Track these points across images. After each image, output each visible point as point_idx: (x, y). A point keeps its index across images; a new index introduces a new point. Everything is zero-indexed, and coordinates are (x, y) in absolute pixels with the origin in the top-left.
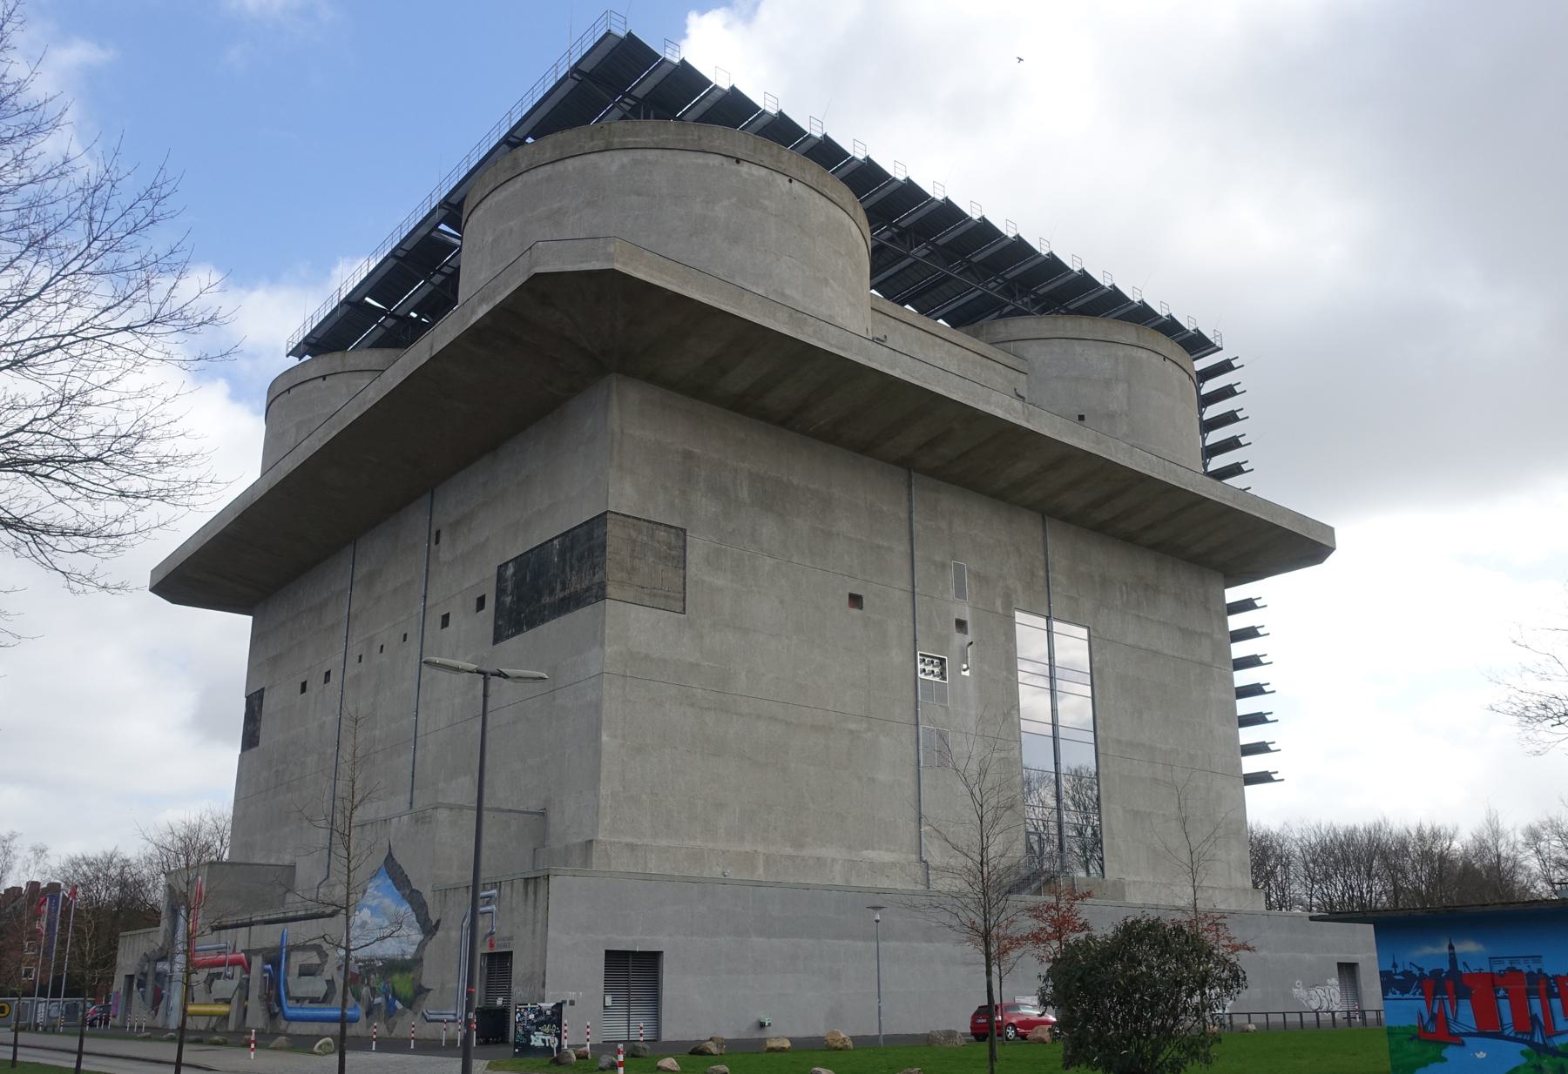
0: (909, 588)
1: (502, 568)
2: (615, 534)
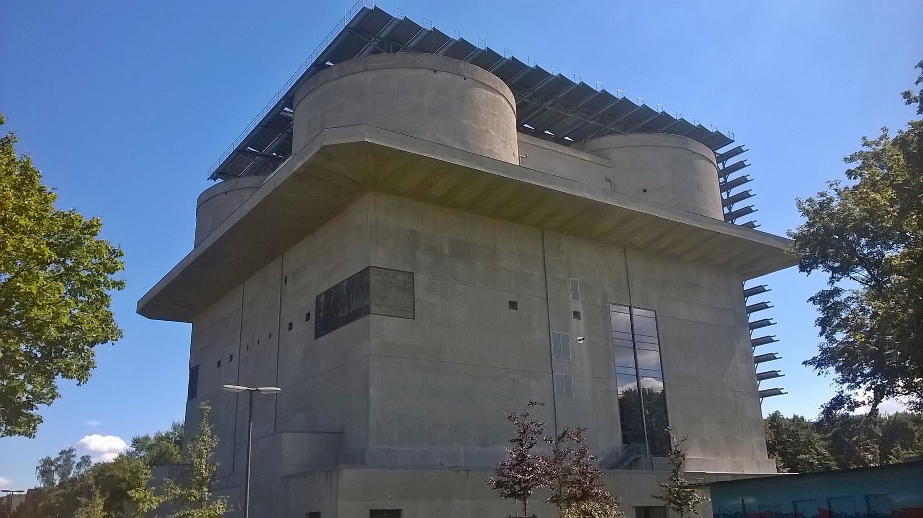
0: (545, 295)
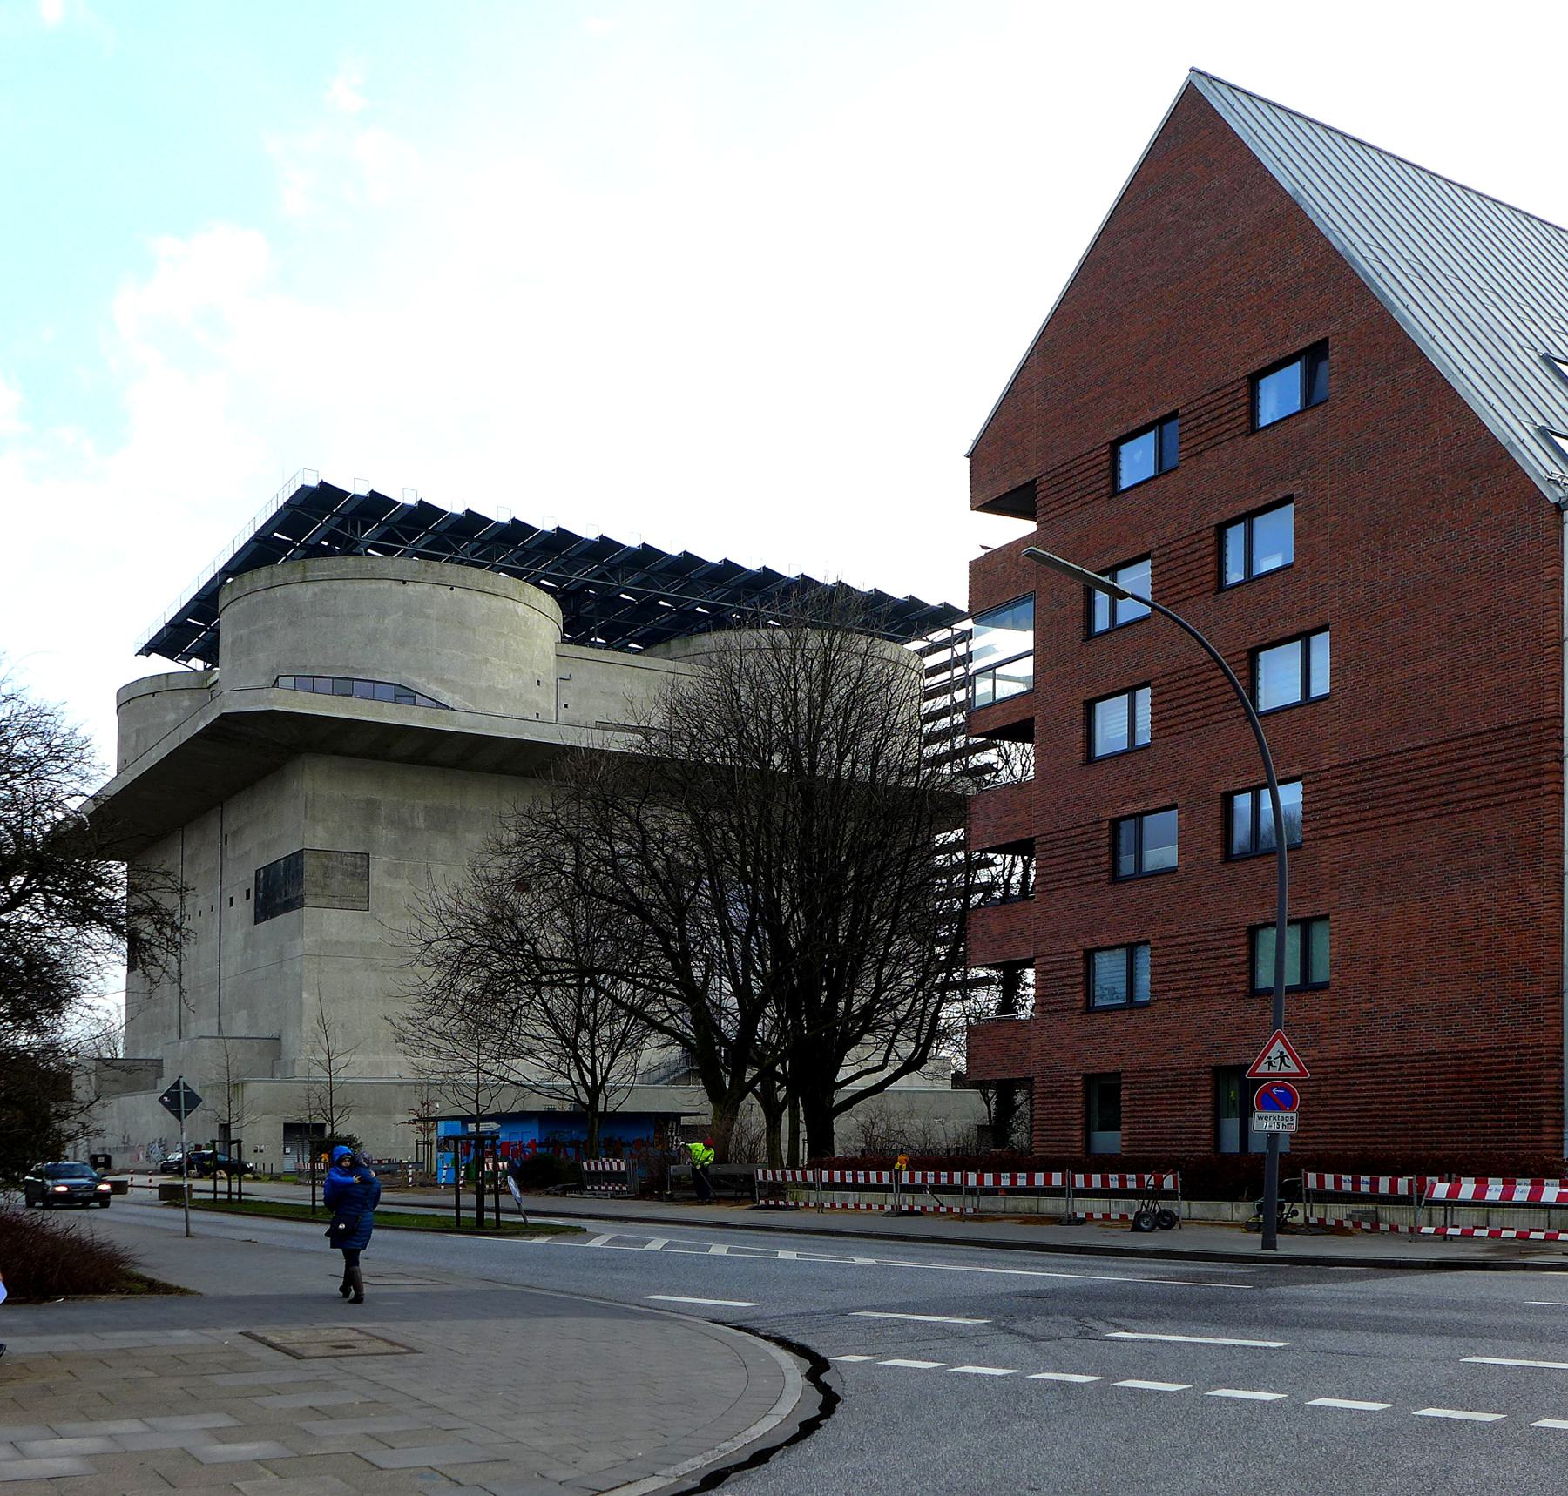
1: (258, 872)
2: (310, 866)
